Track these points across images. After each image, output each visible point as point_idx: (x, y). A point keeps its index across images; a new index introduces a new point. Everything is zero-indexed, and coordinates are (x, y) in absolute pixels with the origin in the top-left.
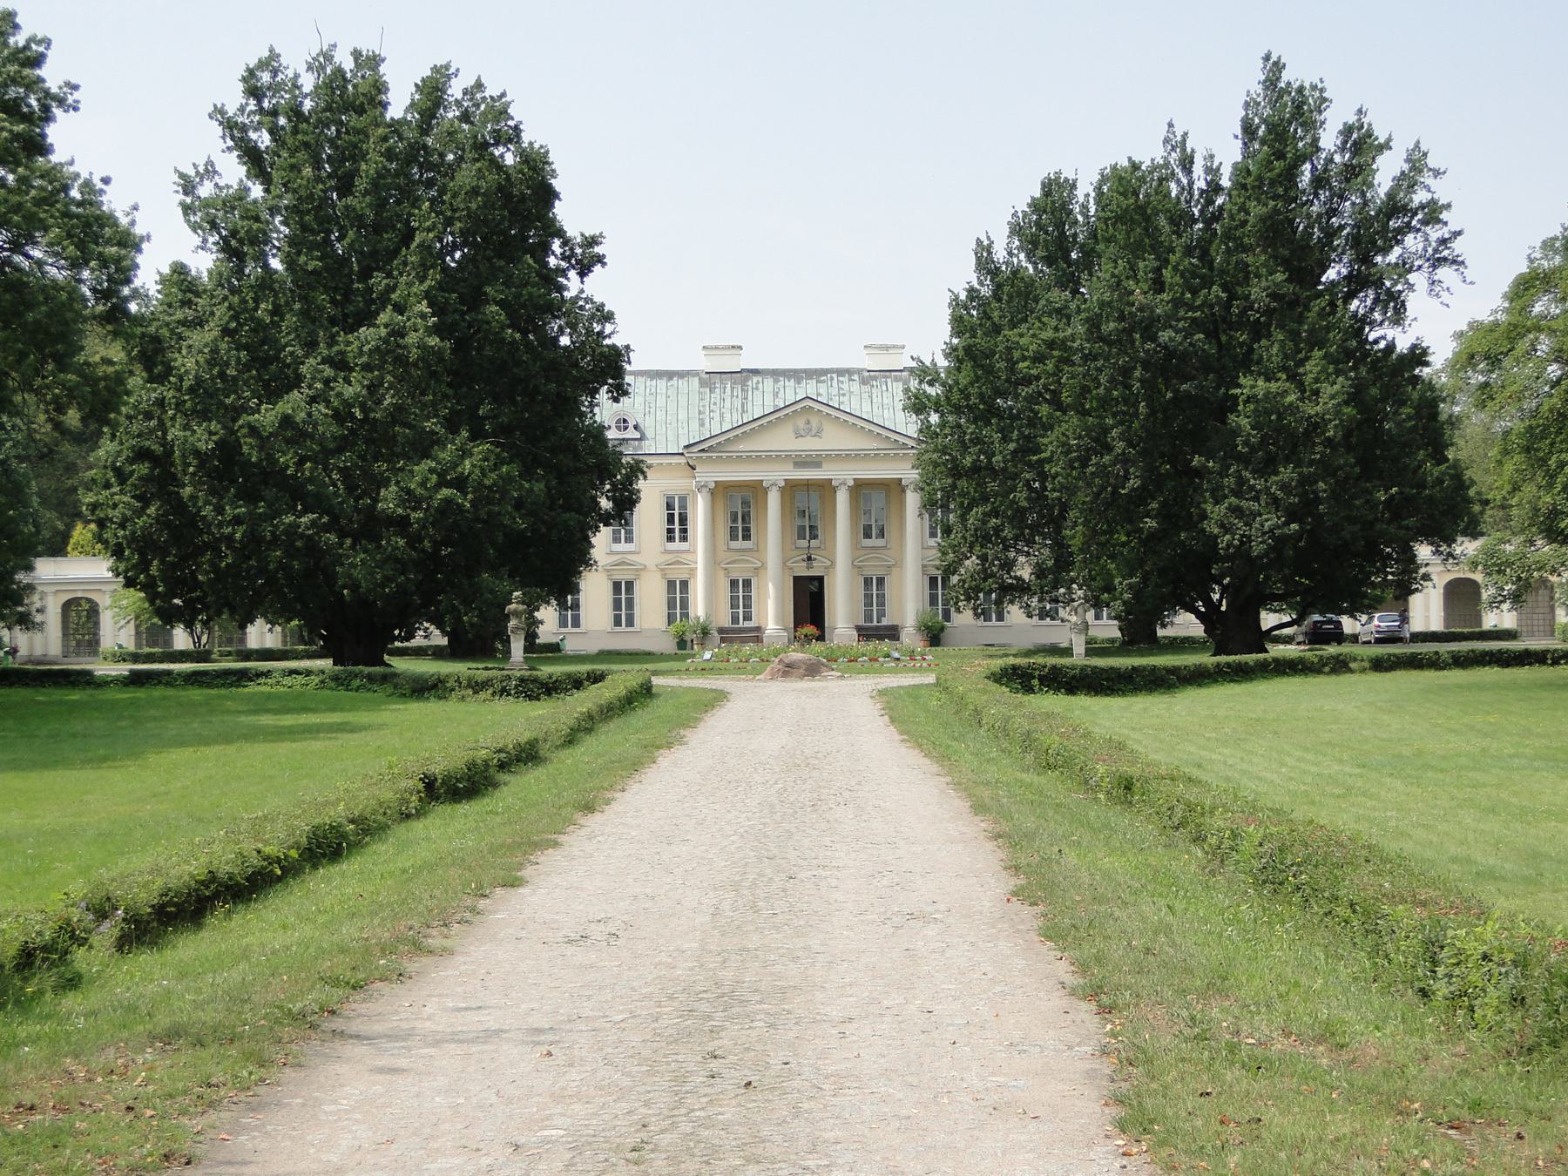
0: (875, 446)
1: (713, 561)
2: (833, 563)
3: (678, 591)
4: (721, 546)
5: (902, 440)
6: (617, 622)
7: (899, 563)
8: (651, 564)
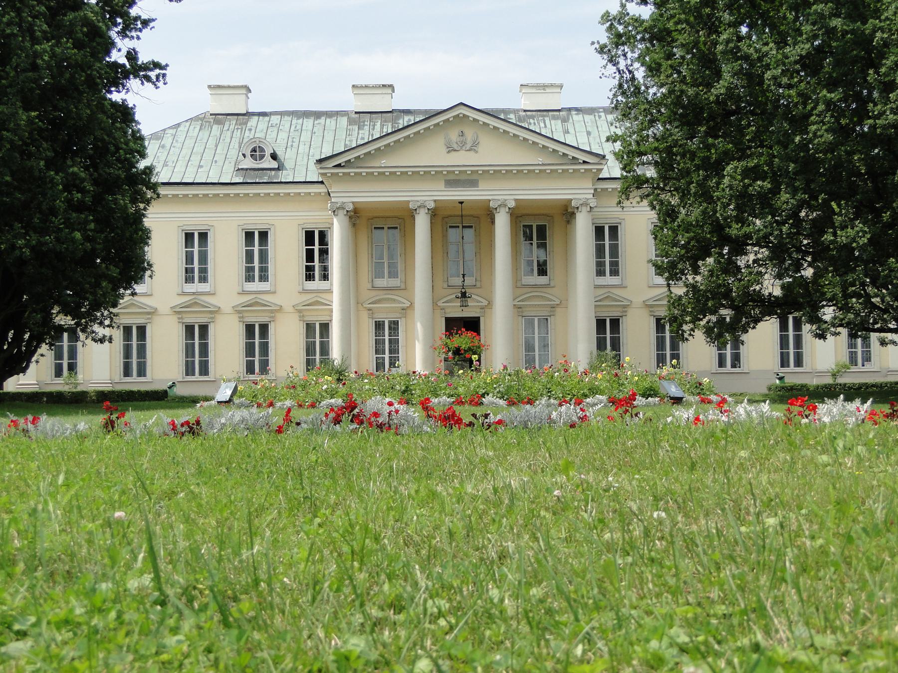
0: (540, 160)
1: (354, 299)
2: (490, 304)
3: (317, 334)
4: (365, 284)
5: (572, 153)
7: (563, 304)
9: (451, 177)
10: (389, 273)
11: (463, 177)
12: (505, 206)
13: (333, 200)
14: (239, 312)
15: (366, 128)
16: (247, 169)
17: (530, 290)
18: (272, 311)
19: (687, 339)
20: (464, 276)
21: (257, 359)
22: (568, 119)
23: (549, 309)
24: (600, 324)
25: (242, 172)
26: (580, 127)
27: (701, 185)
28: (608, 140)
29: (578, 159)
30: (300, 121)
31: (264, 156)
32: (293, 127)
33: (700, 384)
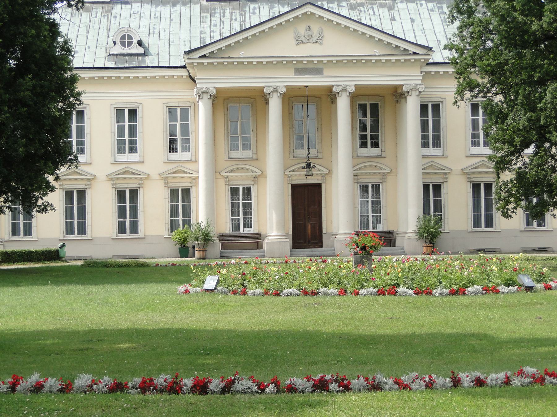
0: (376, 51)
1: (214, 171)
3: (180, 199)
5: (403, 45)
6: (122, 229)
8: (154, 174)
9: (300, 66)
10: (243, 145)
11: (310, 66)
12: (346, 90)
13: (198, 86)
14: (112, 179)
15: (217, 15)
16: (117, 55)
17: (367, 160)
18: (141, 179)
19: (511, 216)
20: (309, 149)
21: (128, 220)
22: (394, 6)
23: (381, 177)
24: (426, 188)
25: (113, 57)
26: (405, 15)
27: (527, 97)
28: (445, 48)
29: (408, 51)
30: (159, 9)
31: (131, 43)
32: (153, 15)
33: (543, 274)
